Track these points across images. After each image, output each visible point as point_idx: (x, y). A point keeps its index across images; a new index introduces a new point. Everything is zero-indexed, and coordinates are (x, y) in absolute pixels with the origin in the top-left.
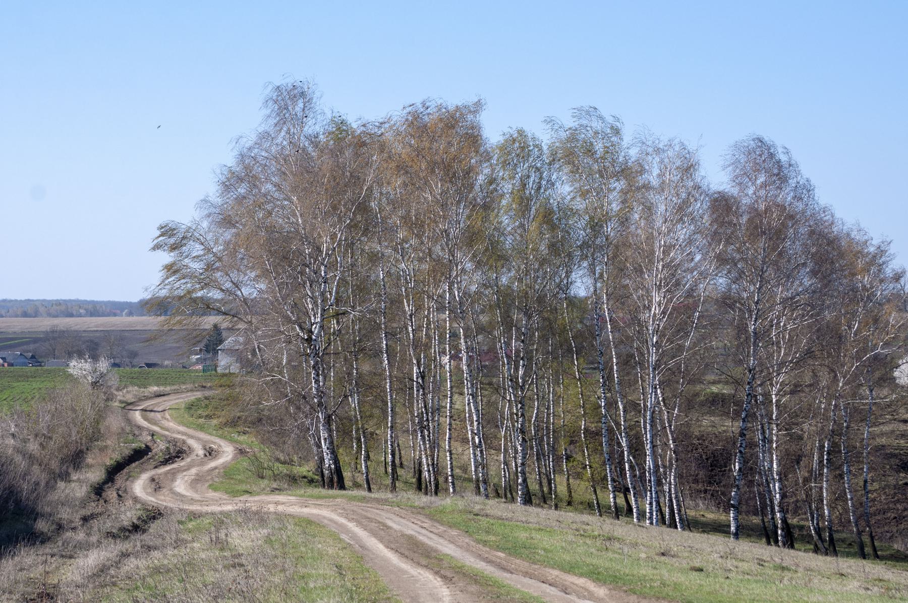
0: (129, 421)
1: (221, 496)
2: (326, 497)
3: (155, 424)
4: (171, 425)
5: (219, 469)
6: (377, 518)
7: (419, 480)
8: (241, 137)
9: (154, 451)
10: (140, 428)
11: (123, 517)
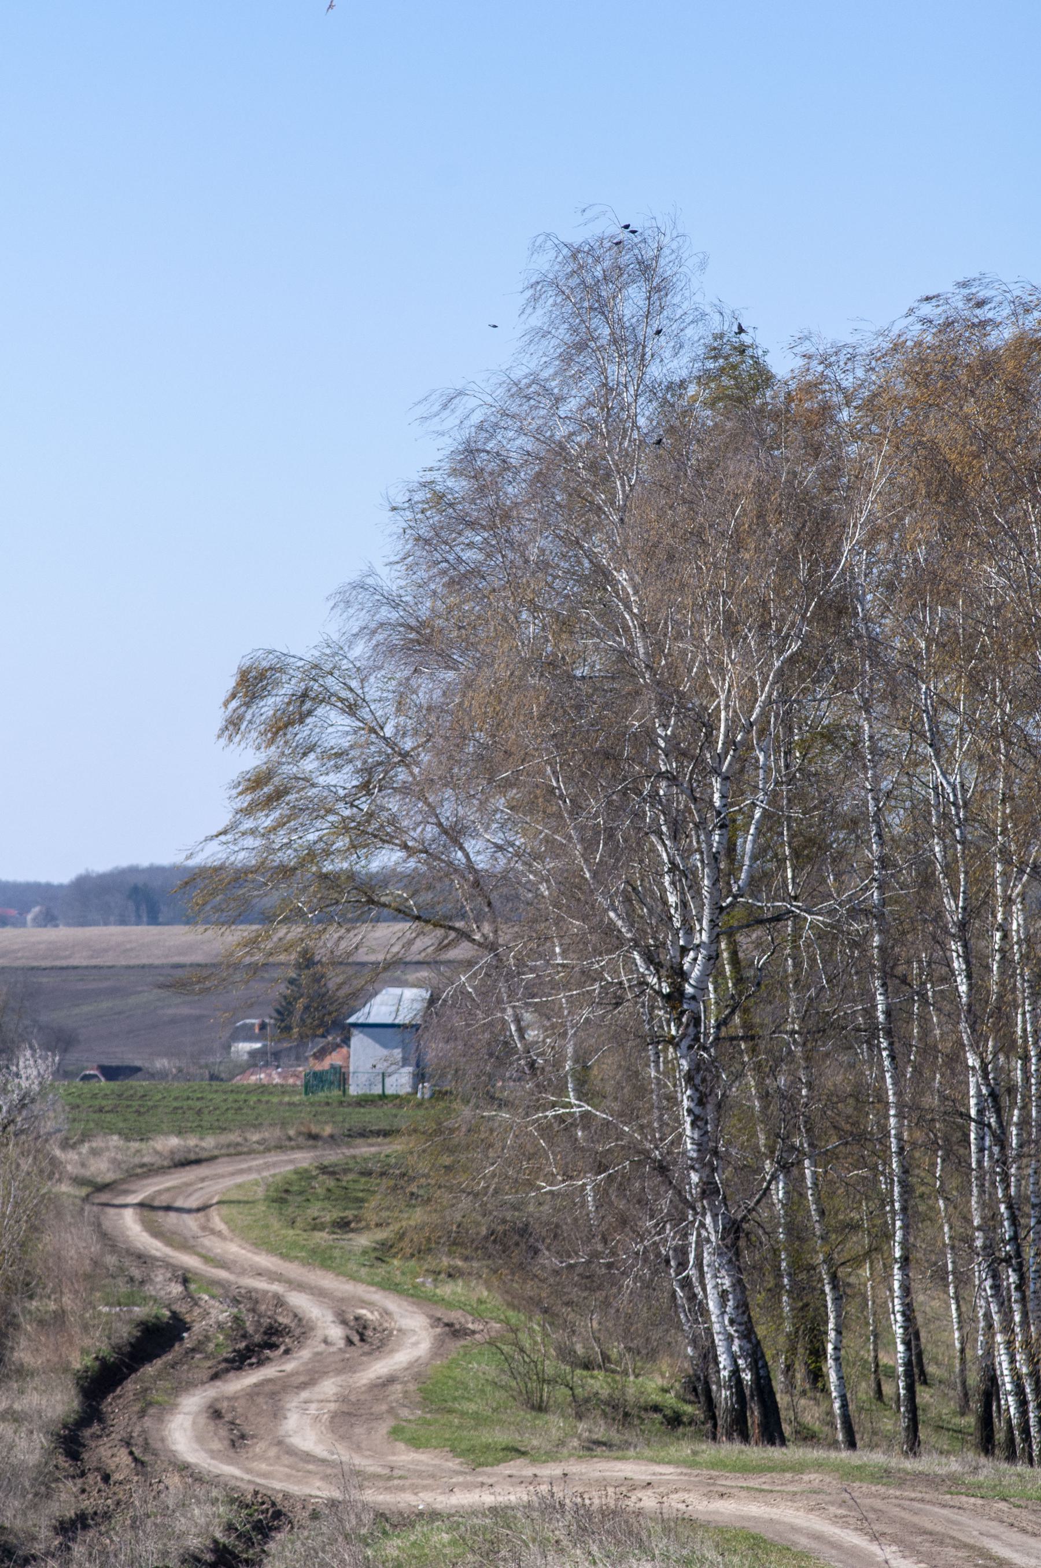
0: (108, 1240)
1: (437, 1462)
2: (771, 1469)
3: (185, 1245)
4: (234, 1249)
5: (405, 1383)
6: (954, 1534)
7: (986, 1422)
8: (461, 393)
9: (196, 1328)
10: (142, 1258)
11: (181, 1524)
